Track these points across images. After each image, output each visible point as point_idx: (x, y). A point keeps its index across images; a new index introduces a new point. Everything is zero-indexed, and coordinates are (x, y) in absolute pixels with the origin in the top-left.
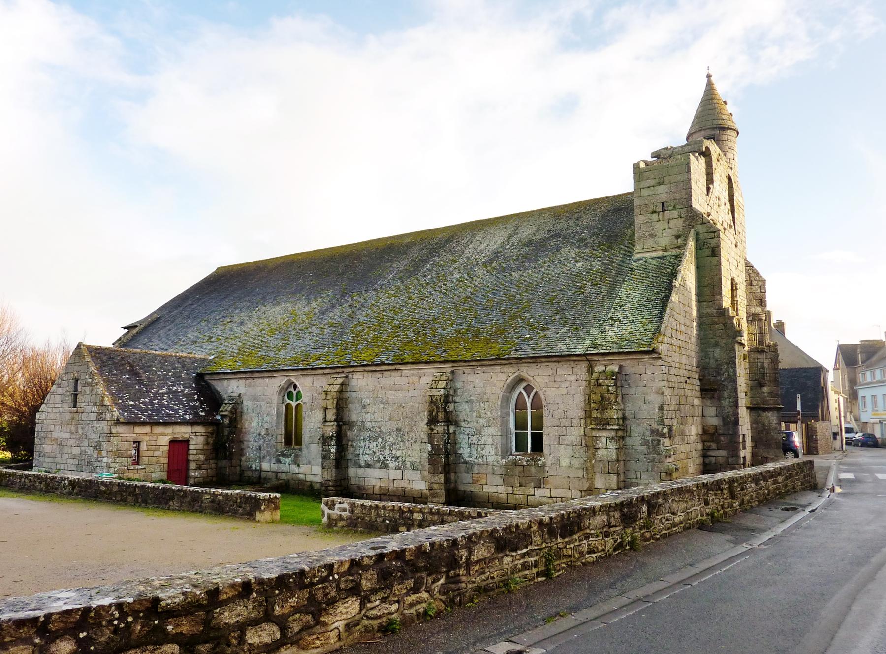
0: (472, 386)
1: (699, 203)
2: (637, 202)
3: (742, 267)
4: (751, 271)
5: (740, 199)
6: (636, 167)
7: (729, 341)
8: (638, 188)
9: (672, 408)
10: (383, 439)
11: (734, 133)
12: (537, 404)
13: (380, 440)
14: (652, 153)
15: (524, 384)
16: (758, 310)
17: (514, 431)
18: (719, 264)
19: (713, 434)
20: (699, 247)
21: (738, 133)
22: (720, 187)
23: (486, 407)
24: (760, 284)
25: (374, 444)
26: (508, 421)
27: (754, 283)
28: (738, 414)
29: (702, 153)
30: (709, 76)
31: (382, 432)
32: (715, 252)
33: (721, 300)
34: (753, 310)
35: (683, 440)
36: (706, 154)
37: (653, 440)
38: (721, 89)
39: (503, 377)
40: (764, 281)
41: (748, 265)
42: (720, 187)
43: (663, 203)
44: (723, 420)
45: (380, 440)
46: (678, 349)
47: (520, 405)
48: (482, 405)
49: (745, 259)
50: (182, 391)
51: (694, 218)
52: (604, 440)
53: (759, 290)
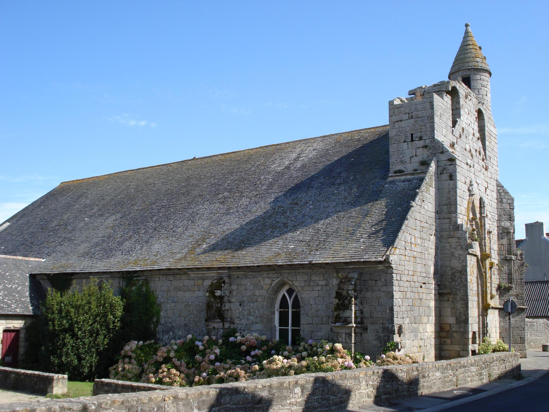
0: (244, 288)
1: (443, 134)
2: (392, 134)
3: (493, 187)
4: (501, 191)
5: (492, 128)
6: (391, 103)
7: (461, 252)
8: (393, 123)
9: (404, 309)
10: (173, 332)
11: (485, 76)
12: (296, 304)
13: (171, 333)
14: (410, 91)
15: (286, 288)
16: (507, 224)
17: (278, 328)
18: (455, 188)
19: (448, 331)
20: (439, 173)
21: (490, 74)
22: (467, 119)
23: (255, 306)
24: (509, 201)
25: (167, 336)
26: (272, 320)
27: (504, 201)
28: (468, 314)
29: (448, 92)
30: (467, 25)
31: (173, 327)
32: (452, 177)
33: (456, 218)
34: (503, 224)
35: (416, 336)
36: (454, 93)
37: (384, 336)
38: (477, 39)
39: (268, 281)
40: (513, 200)
41: (499, 186)
42: (467, 119)
43: (412, 135)
44: (457, 319)
45: (171, 333)
46: (412, 259)
47: (284, 303)
48: (252, 305)
49: (497, 181)
50: (16, 288)
51: (437, 149)
52: (344, 336)
53: (508, 207)
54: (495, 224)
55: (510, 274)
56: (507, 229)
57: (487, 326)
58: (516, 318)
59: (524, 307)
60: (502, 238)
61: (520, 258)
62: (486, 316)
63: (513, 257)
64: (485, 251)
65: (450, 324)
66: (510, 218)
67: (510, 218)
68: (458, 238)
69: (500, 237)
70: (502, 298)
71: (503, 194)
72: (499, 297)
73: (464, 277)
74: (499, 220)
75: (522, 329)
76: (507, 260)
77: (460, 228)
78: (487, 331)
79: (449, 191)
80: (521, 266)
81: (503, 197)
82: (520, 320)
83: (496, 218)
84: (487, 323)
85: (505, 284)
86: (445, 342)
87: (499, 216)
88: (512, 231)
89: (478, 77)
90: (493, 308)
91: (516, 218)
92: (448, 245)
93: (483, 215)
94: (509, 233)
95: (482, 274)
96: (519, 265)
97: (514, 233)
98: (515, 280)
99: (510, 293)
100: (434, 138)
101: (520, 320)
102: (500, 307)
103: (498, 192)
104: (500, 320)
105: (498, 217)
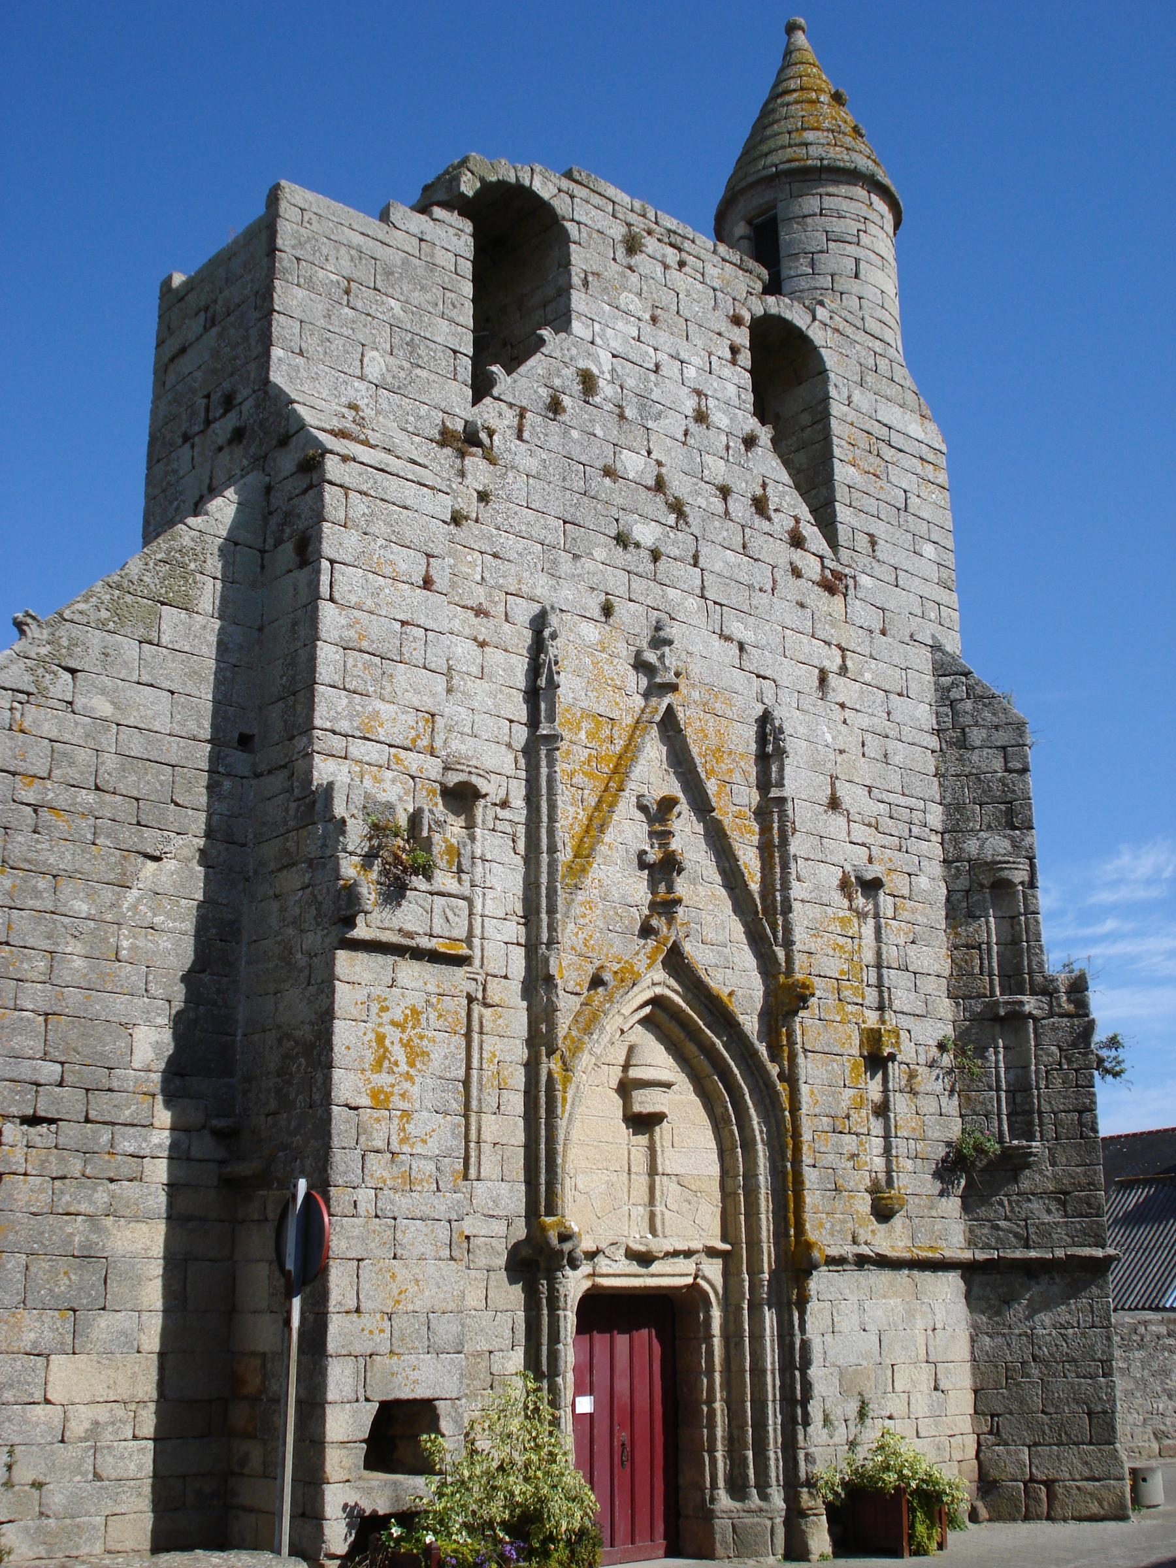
4: (955, 694)
16: (997, 845)
24: (1001, 738)
27: (976, 736)
34: (972, 846)
40: (1019, 727)
53: (998, 764)
54: (933, 848)
55: (1020, 1090)
56: (992, 866)
57: (806, 1363)
58: (1062, 1313)
59: (1099, 1253)
60: (972, 916)
61: (1070, 1008)
62: (802, 1302)
63: (1030, 1004)
64: (790, 971)
65: (264, 1355)
66: (1010, 813)
67: (1010, 813)
68: (310, 863)
69: (960, 910)
70: (982, 1212)
71: (968, 705)
72: (966, 1207)
73: (319, 1076)
74: (953, 831)
75: (1094, 1367)
76: (997, 1019)
77: (319, 806)
78: (807, 1386)
79: (295, 624)
80: (1074, 1045)
81: (968, 720)
82: (1086, 1319)
83: (936, 816)
84: (805, 1345)
85: (996, 1135)
86: (244, 1460)
87: (954, 808)
88: (1019, 876)
89: (811, 204)
90: (836, 1262)
91: (1037, 815)
92: (275, 906)
93: (774, 793)
94: (1002, 887)
95: (769, 1086)
96: (1065, 1037)
97: (1032, 884)
98: (1048, 1119)
99: (1025, 1185)
100: (267, 381)
101: (1086, 1319)
102: (967, 1255)
103: (945, 699)
104: (975, 1326)
105: (948, 814)
